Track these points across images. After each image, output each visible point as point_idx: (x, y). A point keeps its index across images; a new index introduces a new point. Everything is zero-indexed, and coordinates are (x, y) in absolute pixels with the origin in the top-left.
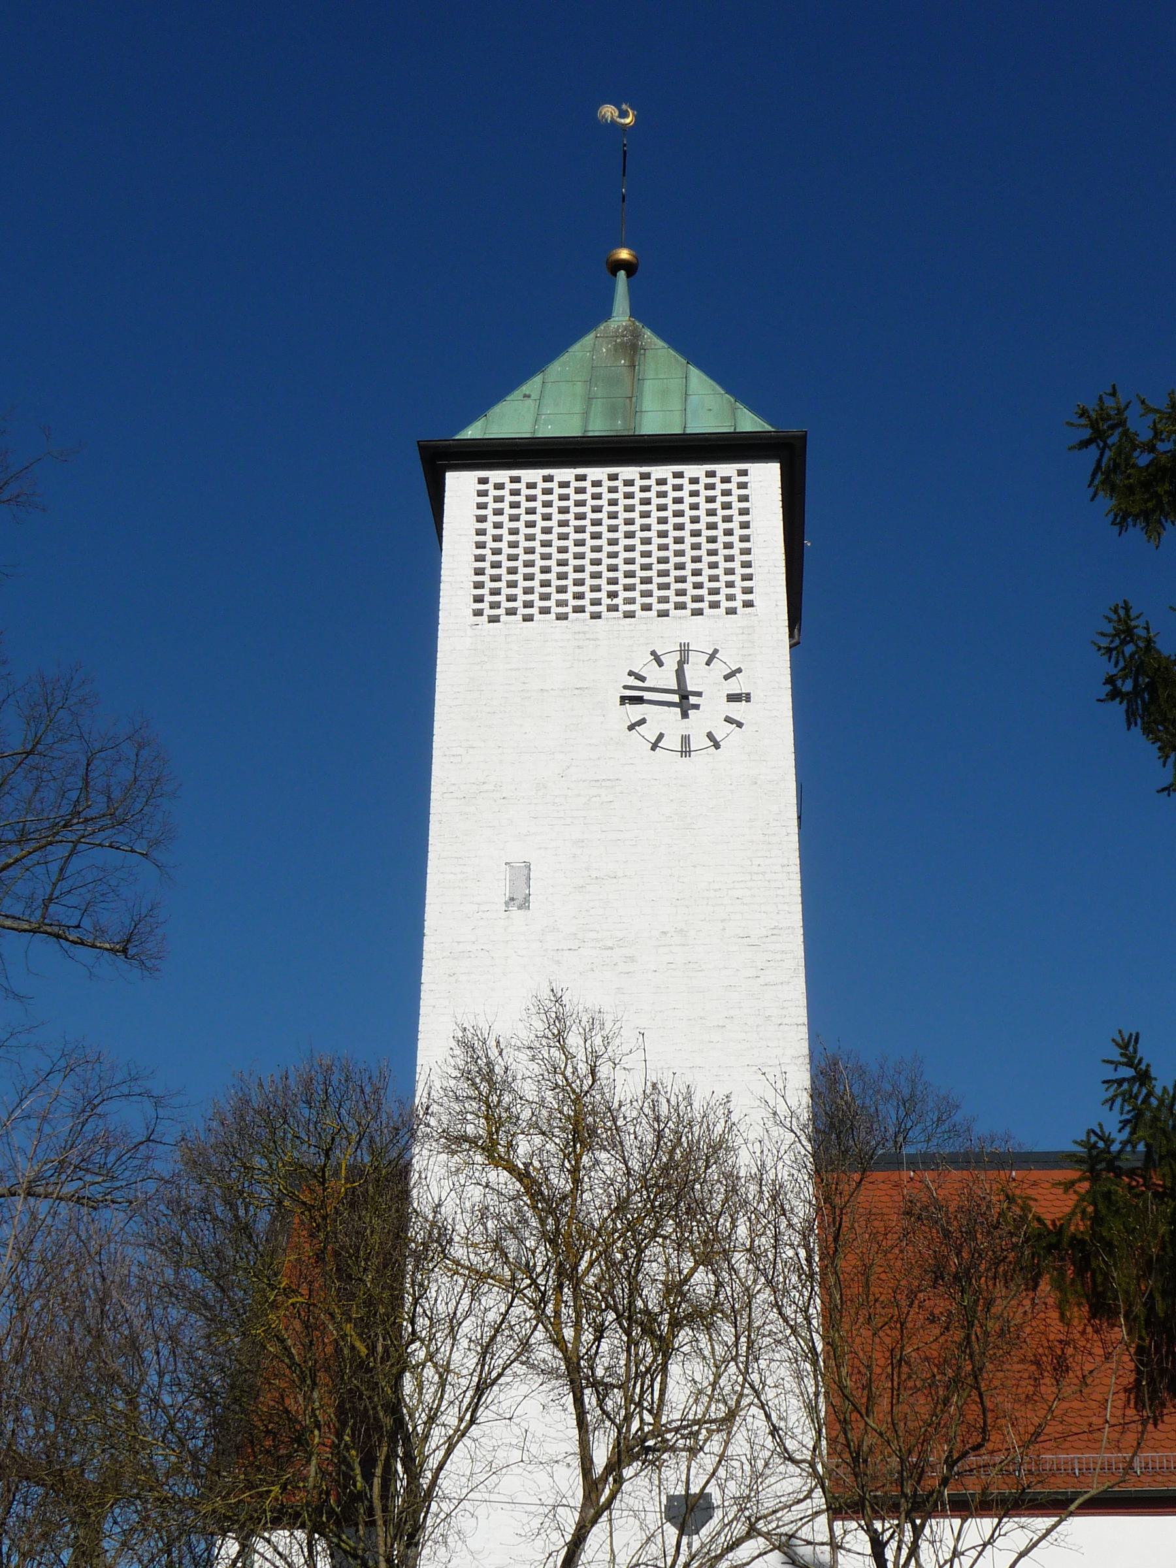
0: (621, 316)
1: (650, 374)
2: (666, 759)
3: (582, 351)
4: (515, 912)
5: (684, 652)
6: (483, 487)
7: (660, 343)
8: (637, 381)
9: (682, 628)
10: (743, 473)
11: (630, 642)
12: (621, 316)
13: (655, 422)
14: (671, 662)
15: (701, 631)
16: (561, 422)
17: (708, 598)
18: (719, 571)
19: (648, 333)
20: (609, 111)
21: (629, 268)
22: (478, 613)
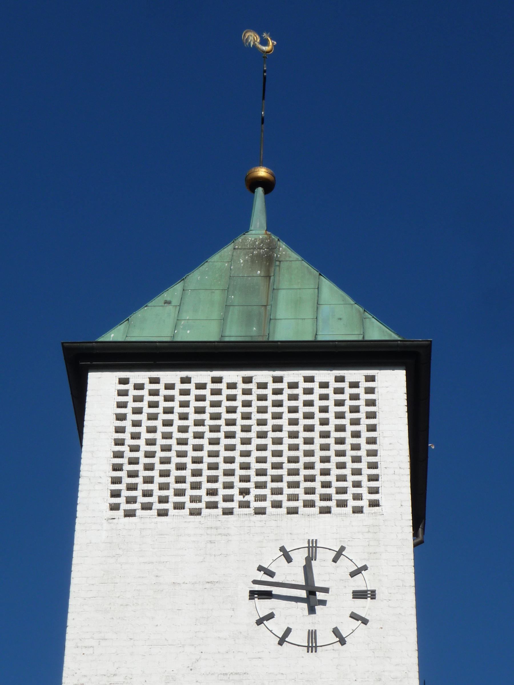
2: (329, 655)
3: (220, 261)
5: (312, 548)
7: (294, 256)
8: (272, 291)
9: (310, 526)
13: (289, 328)
14: (299, 558)
15: (329, 529)
16: (200, 328)
17: (336, 497)
18: (347, 472)
19: (283, 246)
20: (252, 37)
21: (267, 185)
22: (115, 507)
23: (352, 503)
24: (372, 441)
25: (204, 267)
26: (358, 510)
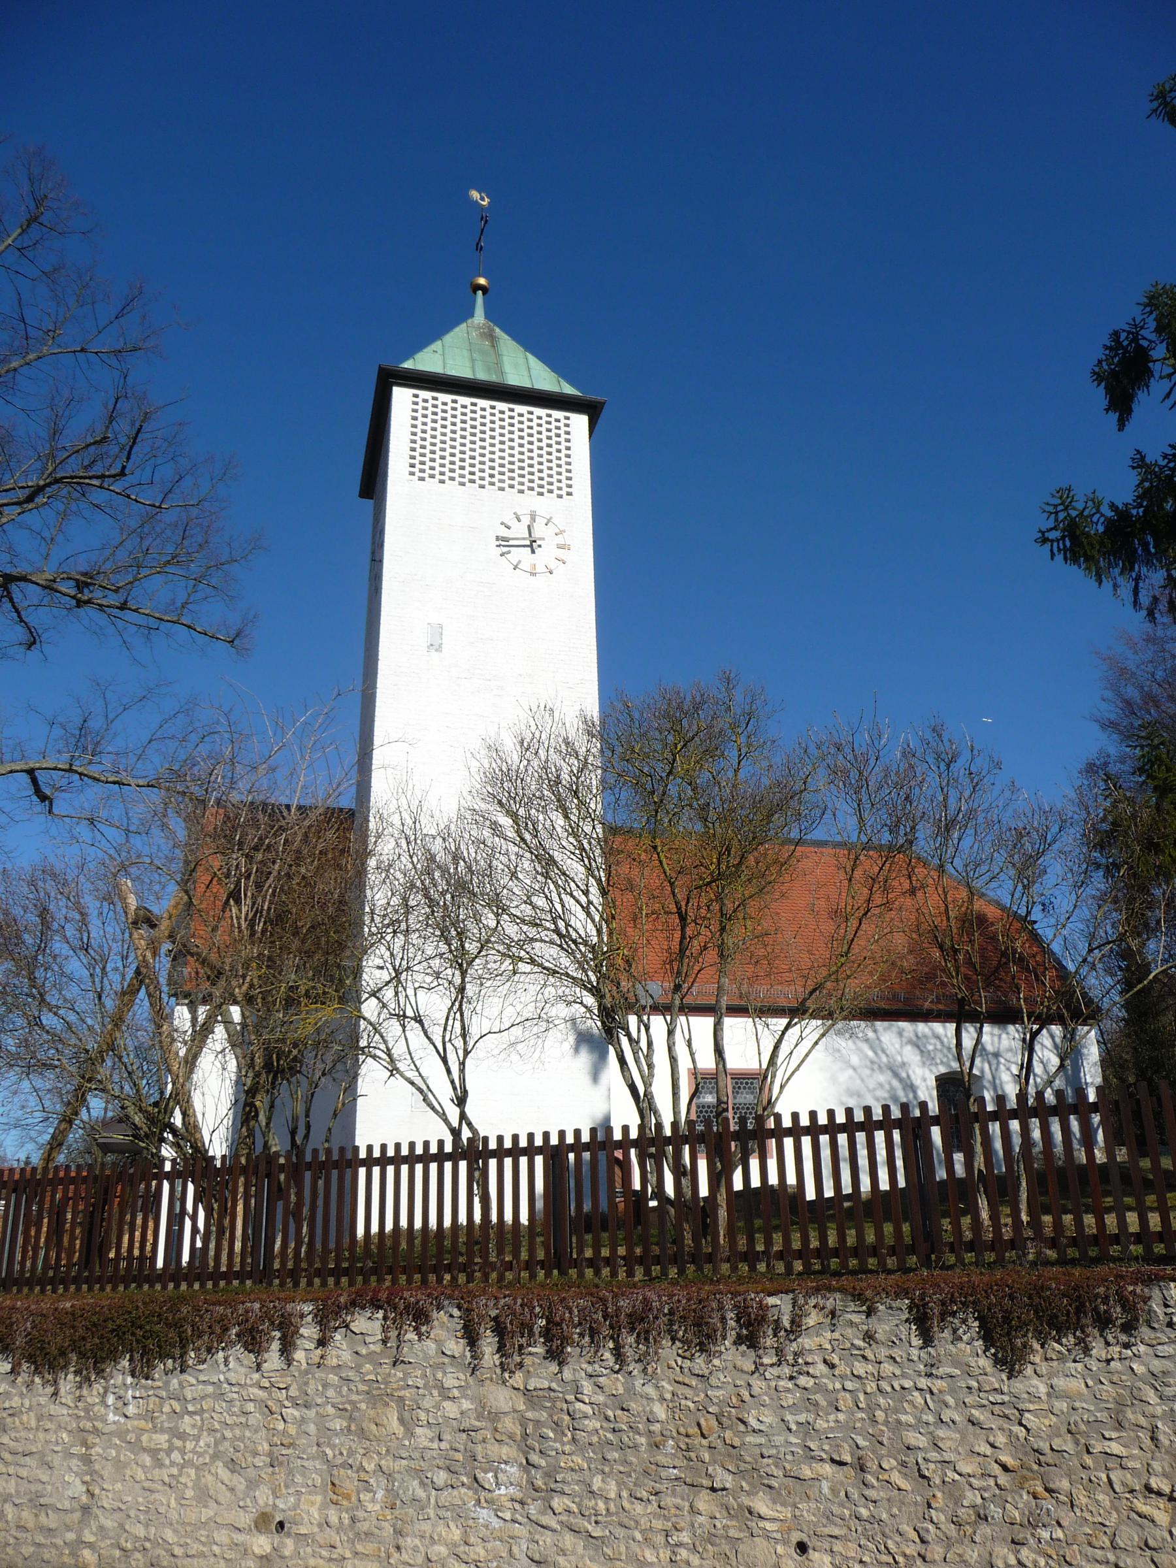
0: (479, 316)
1: (505, 353)
2: (541, 580)
3: (460, 331)
4: (434, 654)
5: (533, 517)
6: (415, 400)
7: (506, 337)
8: (498, 356)
9: (530, 502)
10: (568, 418)
11: (499, 507)
12: (479, 316)
13: (515, 378)
14: (526, 520)
15: (545, 505)
16: (459, 368)
17: (547, 487)
18: (456, 467)
19: (497, 330)
20: (475, 195)
21: (485, 290)
22: (412, 474)
23: (518, 487)
24: (568, 456)
25: (452, 334)
26: (560, 496)
